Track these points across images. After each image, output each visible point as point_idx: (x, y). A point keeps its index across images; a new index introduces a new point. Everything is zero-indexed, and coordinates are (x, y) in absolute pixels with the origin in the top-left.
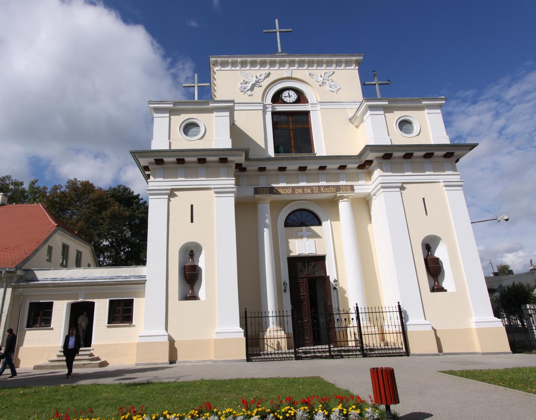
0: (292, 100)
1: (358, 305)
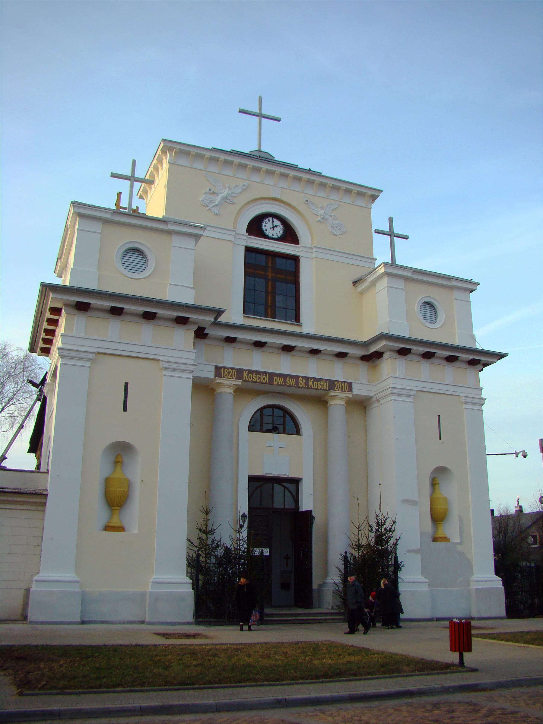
0: (277, 234)
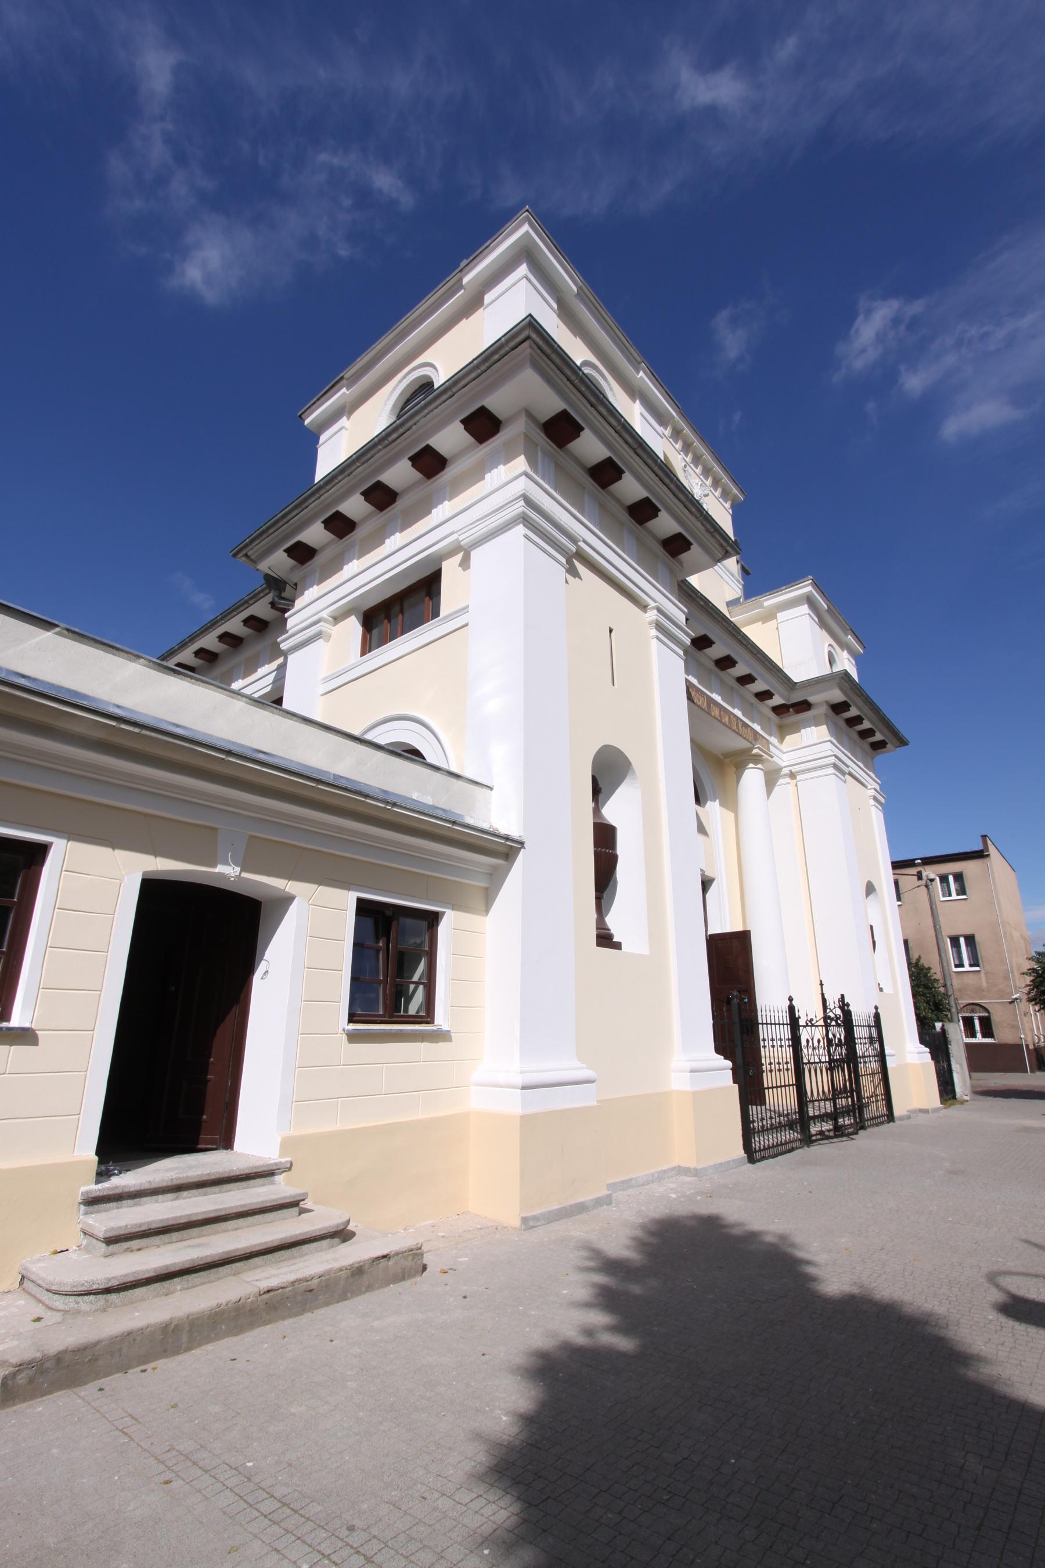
1: (879, 1010)
